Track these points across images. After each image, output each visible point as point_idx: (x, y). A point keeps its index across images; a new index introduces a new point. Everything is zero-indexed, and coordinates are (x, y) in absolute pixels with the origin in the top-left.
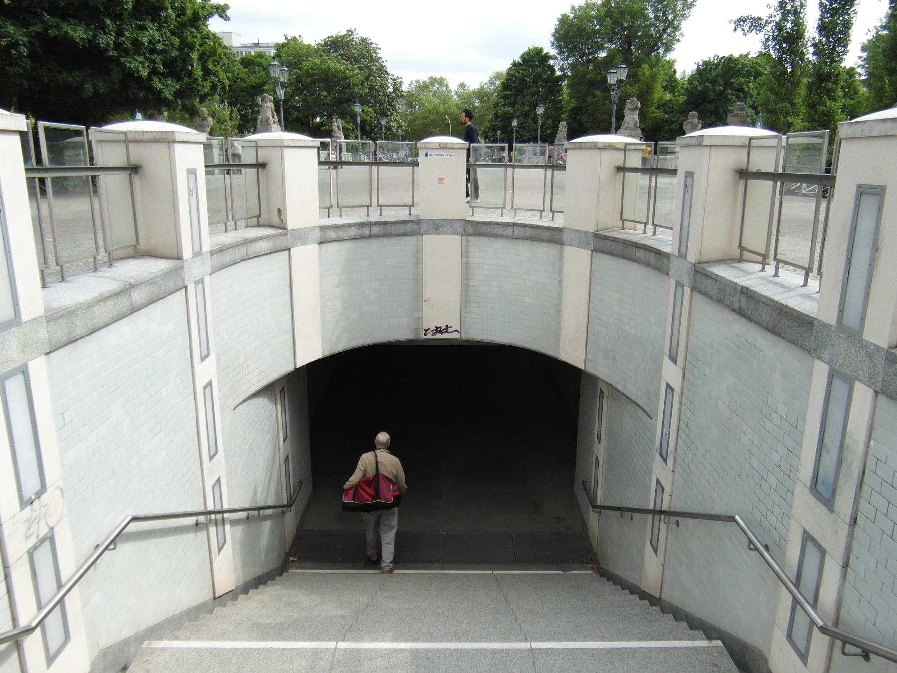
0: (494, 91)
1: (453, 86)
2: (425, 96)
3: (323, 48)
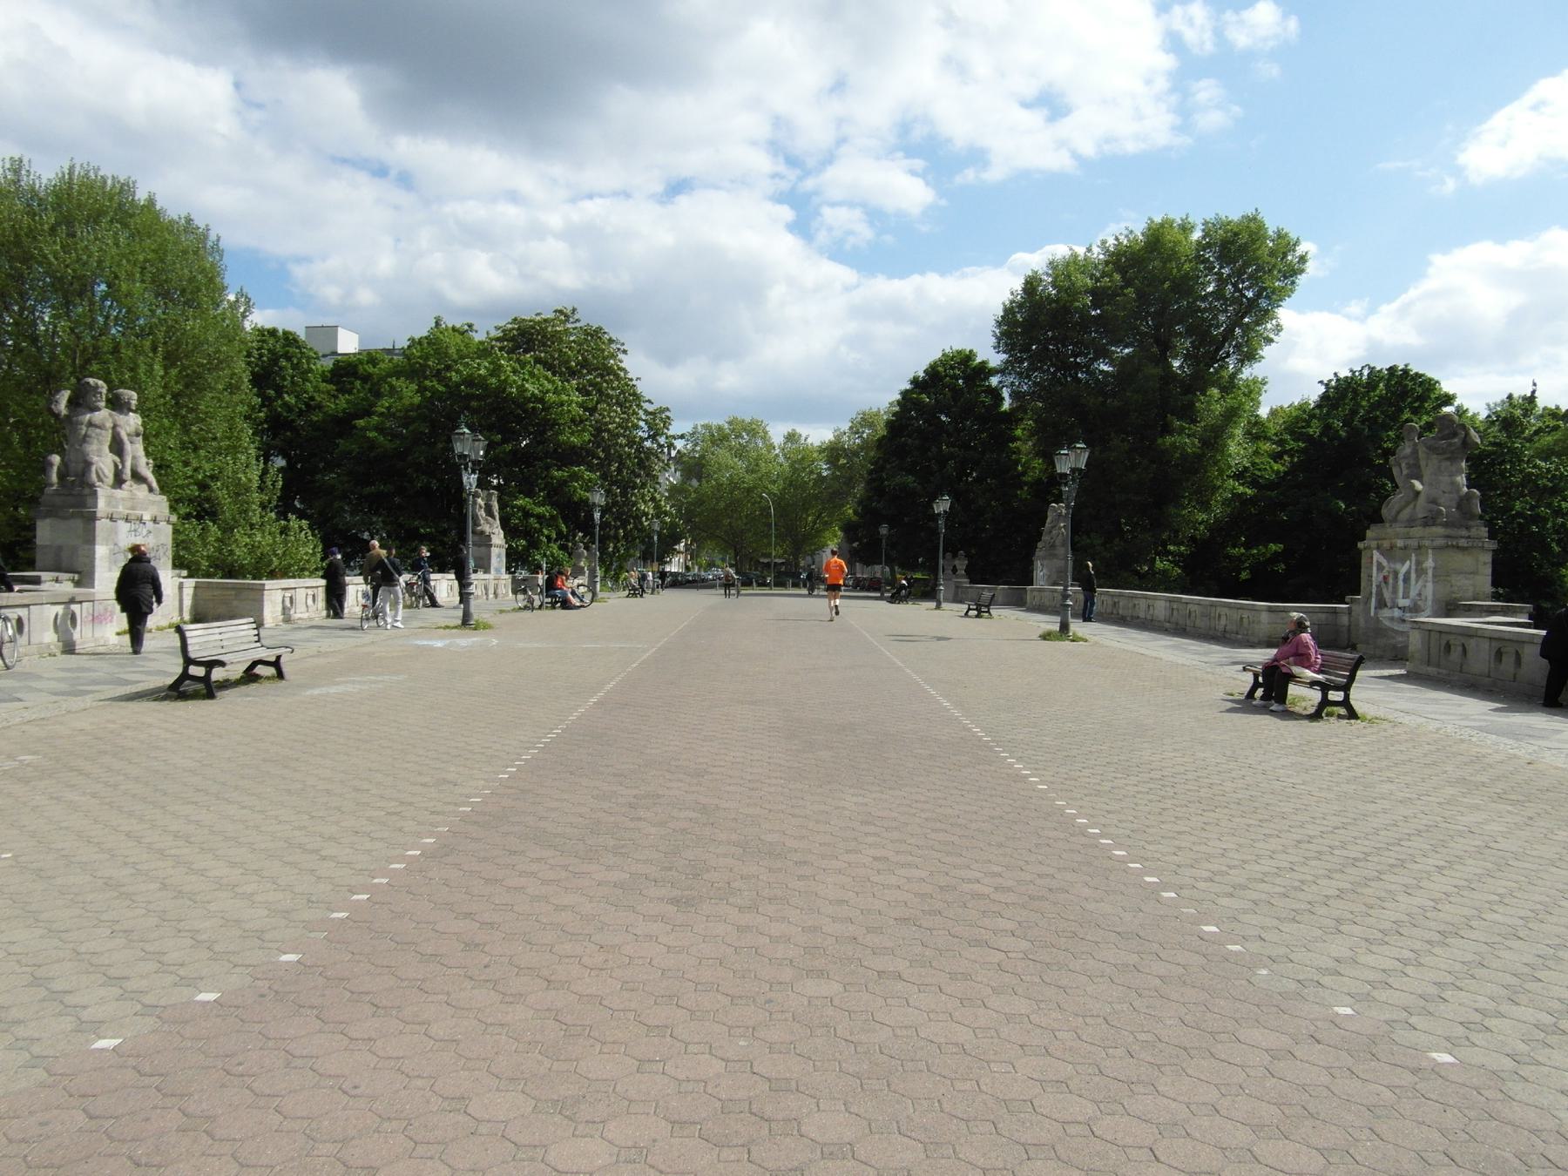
0: (861, 448)
1: (777, 434)
2: (722, 455)
3: (498, 344)
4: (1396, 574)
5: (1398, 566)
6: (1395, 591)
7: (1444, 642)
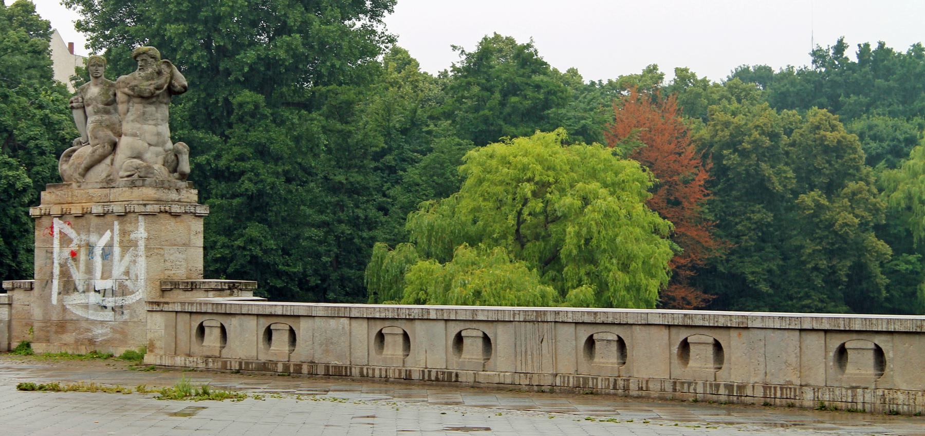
4: (90, 248)
5: (93, 238)
6: (89, 270)
7: (195, 325)
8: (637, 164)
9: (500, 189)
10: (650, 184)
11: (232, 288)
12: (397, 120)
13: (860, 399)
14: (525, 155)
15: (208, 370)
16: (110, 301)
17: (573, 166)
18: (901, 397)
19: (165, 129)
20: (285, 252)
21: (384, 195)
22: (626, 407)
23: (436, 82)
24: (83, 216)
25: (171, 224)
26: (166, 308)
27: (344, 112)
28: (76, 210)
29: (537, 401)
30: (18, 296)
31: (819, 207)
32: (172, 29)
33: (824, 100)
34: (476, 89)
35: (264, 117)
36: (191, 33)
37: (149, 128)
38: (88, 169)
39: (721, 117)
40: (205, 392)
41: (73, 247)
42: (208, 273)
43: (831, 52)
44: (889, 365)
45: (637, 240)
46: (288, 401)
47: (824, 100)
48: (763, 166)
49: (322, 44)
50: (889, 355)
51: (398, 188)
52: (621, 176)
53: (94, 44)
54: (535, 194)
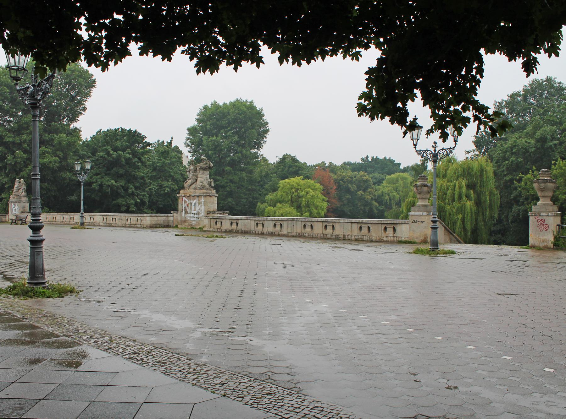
4: (191, 204)
5: (192, 201)
6: (191, 209)
7: (215, 221)
8: (319, 184)
9: (287, 190)
10: (323, 189)
11: (223, 213)
12: (263, 174)
13: (364, 238)
14: (293, 182)
15: (218, 232)
16: (196, 216)
17: (304, 185)
18: (373, 238)
19: (208, 176)
20: (237, 205)
21: (260, 192)
22: (312, 240)
23: (273, 165)
24: (189, 196)
25: (209, 198)
26: (208, 217)
27: (251, 172)
28: (188, 195)
29: (292, 239)
30: (175, 214)
31: (362, 194)
32: (210, 153)
33: (363, 170)
34: (282, 167)
35: (232, 173)
36: (215, 153)
37: (204, 176)
38: (190, 185)
39: (340, 173)
40: (217, 236)
41: (187, 203)
42: (218, 209)
43: (365, 158)
44: (371, 230)
45: (319, 202)
46: (236, 239)
47: (363, 170)
48: (349, 185)
49: (246, 156)
50: (371, 228)
51: (264, 190)
52: (316, 187)
53: (192, 156)
54: (296, 191)
